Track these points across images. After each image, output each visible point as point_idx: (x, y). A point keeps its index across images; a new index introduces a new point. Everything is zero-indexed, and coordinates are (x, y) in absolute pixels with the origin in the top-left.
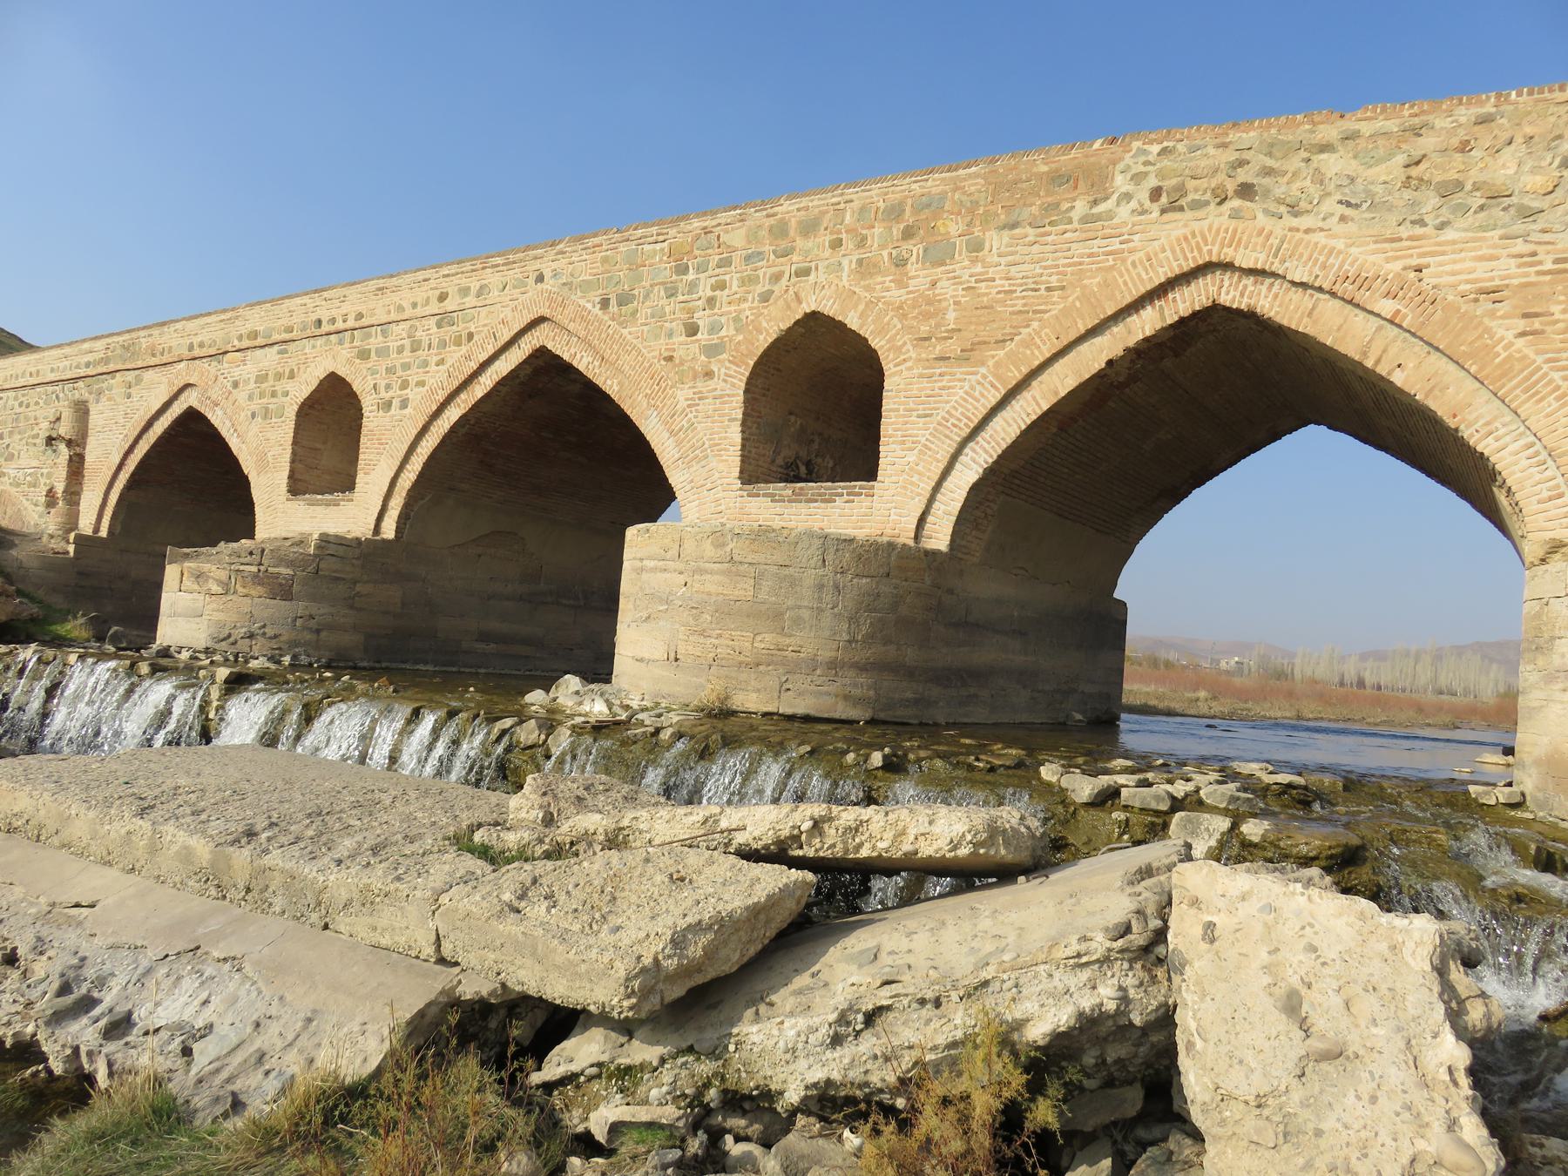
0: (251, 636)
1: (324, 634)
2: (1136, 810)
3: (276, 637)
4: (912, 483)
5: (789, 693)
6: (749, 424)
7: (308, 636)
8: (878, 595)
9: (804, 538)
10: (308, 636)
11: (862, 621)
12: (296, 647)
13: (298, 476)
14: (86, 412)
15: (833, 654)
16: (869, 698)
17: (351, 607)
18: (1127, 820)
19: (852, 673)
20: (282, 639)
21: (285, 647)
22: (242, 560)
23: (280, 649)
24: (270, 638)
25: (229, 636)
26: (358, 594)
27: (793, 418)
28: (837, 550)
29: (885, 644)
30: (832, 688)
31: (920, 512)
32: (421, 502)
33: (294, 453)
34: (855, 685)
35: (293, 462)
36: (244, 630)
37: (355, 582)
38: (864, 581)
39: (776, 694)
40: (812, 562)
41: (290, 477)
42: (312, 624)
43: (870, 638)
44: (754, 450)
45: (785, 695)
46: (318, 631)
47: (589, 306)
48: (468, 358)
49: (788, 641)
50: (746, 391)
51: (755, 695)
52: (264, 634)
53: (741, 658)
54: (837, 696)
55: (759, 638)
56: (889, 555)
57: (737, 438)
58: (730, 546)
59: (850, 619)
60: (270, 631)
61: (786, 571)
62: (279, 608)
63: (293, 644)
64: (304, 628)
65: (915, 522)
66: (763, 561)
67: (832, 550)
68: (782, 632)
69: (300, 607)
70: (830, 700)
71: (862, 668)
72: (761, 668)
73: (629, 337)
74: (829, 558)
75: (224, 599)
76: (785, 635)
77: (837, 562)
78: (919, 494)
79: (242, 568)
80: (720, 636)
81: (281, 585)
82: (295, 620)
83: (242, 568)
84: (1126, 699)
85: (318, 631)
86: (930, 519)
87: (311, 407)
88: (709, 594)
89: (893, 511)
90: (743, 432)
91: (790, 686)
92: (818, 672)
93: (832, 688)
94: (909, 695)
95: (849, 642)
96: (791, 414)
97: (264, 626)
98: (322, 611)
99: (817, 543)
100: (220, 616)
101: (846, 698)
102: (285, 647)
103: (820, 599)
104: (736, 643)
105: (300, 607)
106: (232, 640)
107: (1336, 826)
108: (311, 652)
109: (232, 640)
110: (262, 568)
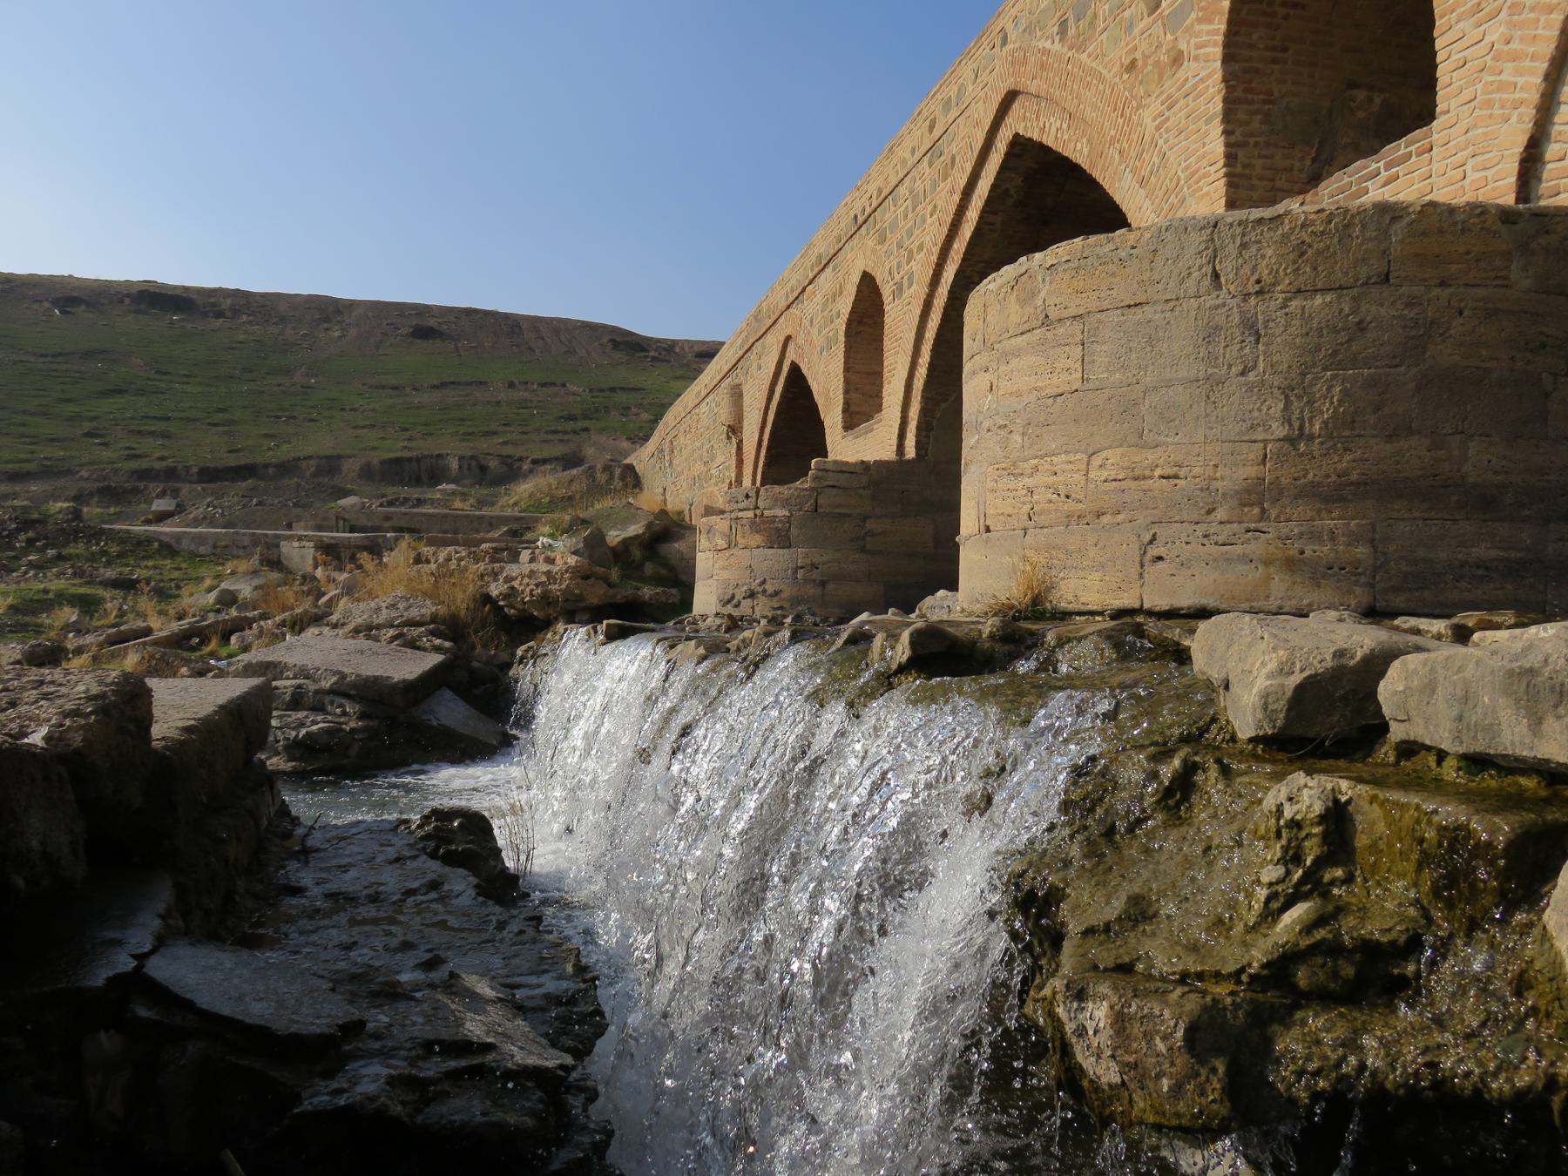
0: (752, 595)
1: (830, 586)
2: (1450, 771)
3: (776, 594)
4: (1502, 87)
5: (1161, 565)
6: (1241, 116)
7: (811, 590)
8: (1361, 327)
9: (1169, 236)
10: (811, 590)
11: (1319, 389)
12: (799, 605)
13: (853, 408)
14: (741, 395)
15: (1252, 471)
16: (1357, 563)
17: (863, 550)
18: (1337, 817)
19: (1303, 509)
20: (784, 595)
21: (787, 605)
22: (741, 506)
23: (781, 608)
24: (771, 596)
25: (733, 596)
26: (871, 533)
27: (1361, 95)
28: (1244, 246)
29: (1390, 438)
30: (1256, 547)
31: (1523, 140)
32: (944, 405)
33: (847, 382)
34: (1314, 536)
35: (846, 392)
36: (745, 588)
37: (865, 518)
38: (1319, 300)
39: (1134, 570)
40: (1190, 284)
41: (845, 411)
42: (815, 575)
43: (1344, 429)
44: (1259, 163)
45: (1152, 571)
46: (823, 584)
47: (1048, 45)
48: (952, 192)
49: (1152, 456)
50: (1227, 59)
51: (1097, 576)
52: (764, 591)
53: (1071, 506)
54: (1267, 563)
55: (1096, 461)
56: (1386, 233)
57: (1216, 145)
58: (1042, 294)
59: (1287, 391)
60: (770, 588)
61: (1138, 315)
62: (776, 560)
63: (796, 601)
64: (806, 581)
65: (1514, 167)
66: (1094, 305)
67: (1232, 249)
68: (1141, 441)
69: (799, 554)
70: (1255, 574)
71: (1331, 495)
72: (1105, 519)
73: (1088, 61)
74: (1226, 268)
75: (727, 553)
76: (1146, 446)
77: (1246, 270)
78: (1517, 104)
79: (740, 514)
80: (1036, 469)
81: (777, 530)
82: (795, 571)
83: (740, 514)
84: (1501, 189)
85: (823, 584)
86: (1552, 150)
87: (860, 322)
88: (1019, 395)
89: (1468, 167)
90: (1226, 132)
91: (1161, 551)
92: (1221, 514)
93: (1256, 547)
94: (1480, 551)
95: (1291, 440)
96: (1353, 85)
97: (764, 582)
98: (825, 559)
99: (1197, 239)
100: (725, 575)
101: (1292, 565)
102: (787, 605)
103: (1211, 359)
104: (1060, 478)
105: (799, 554)
106: (735, 601)
107: (27, 631)
108: (817, 610)
109: (735, 601)
110: (758, 512)
